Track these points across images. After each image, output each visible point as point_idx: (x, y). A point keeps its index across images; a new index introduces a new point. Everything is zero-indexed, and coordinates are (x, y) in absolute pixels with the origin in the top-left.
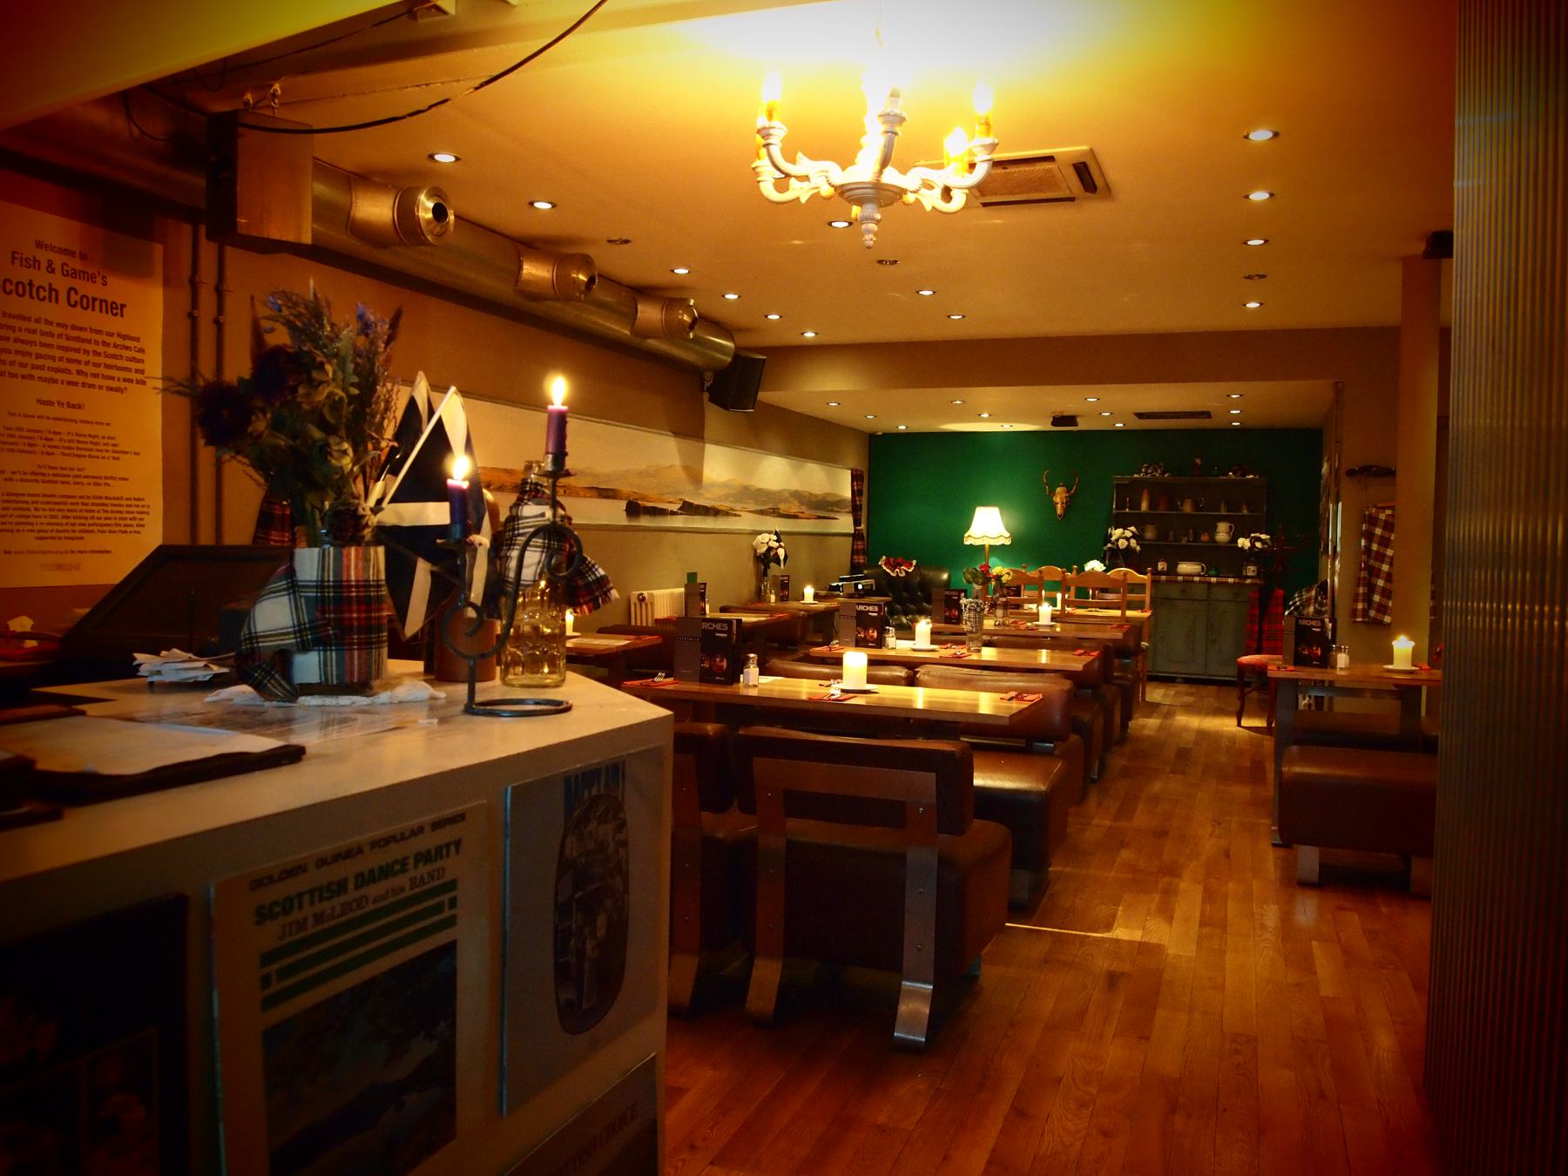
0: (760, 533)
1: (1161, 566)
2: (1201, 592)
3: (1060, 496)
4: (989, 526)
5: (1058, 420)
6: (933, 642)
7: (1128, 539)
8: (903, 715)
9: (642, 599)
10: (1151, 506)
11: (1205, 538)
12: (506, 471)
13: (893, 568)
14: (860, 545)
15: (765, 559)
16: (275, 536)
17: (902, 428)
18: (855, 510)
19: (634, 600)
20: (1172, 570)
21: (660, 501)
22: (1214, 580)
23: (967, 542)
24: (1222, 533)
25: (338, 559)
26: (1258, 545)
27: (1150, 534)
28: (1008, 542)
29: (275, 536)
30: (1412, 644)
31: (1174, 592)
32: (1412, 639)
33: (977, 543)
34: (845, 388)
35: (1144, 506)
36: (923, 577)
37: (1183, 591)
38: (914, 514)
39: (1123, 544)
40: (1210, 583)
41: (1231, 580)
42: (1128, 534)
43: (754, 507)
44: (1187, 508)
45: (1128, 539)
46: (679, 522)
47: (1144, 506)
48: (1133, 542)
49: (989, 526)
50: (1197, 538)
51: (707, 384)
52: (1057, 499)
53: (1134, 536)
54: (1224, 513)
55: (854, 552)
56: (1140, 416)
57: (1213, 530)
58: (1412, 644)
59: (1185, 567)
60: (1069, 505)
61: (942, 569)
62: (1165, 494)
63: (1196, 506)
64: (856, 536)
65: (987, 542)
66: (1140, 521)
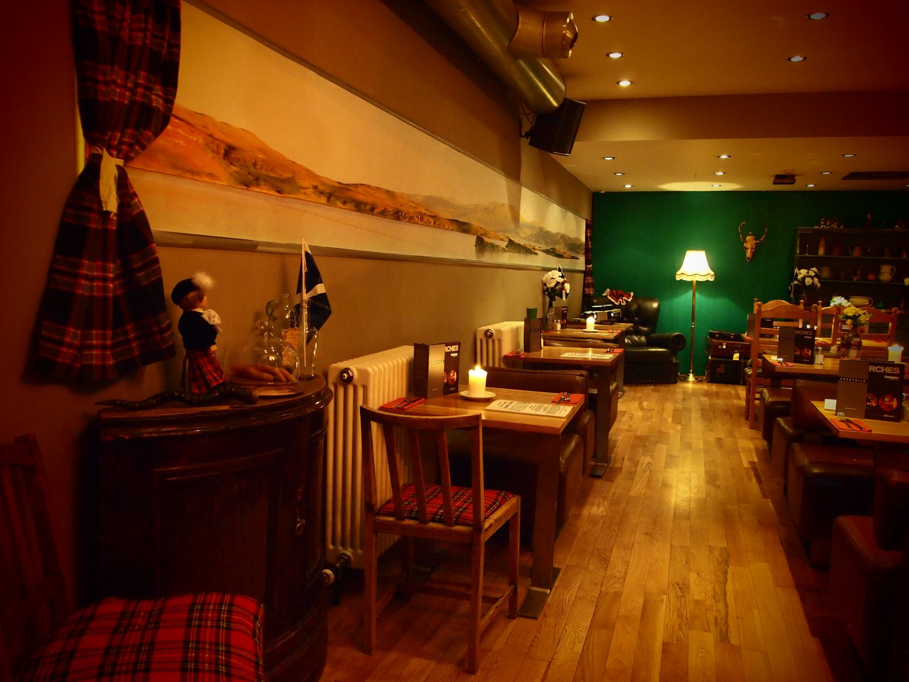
0: (550, 270)
3: (750, 243)
4: (696, 265)
5: (780, 179)
7: (812, 278)
9: (488, 335)
10: (826, 253)
11: (871, 277)
12: (388, 192)
13: (617, 298)
14: (590, 280)
15: (553, 293)
16: (88, 268)
17: (628, 186)
18: (587, 252)
19: (480, 336)
21: (496, 238)
24: (886, 274)
27: (825, 274)
28: (711, 279)
29: (88, 268)
30: (902, 348)
32: (901, 345)
33: (684, 278)
34: (641, 139)
35: (821, 252)
36: (639, 307)
38: (630, 256)
39: (808, 281)
42: (812, 273)
43: (544, 247)
44: (857, 253)
45: (812, 278)
46: (506, 258)
47: (821, 252)
48: (816, 280)
49: (696, 265)
51: (526, 127)
53: (817, 275)
54: (887, 257)
55: (585, 285)
56: (853, 176)
57: (878, 272)
58: (902, 348)
61: (652, 299)
64: (586, 273)
65: (694, 279)
66: (817, 262)
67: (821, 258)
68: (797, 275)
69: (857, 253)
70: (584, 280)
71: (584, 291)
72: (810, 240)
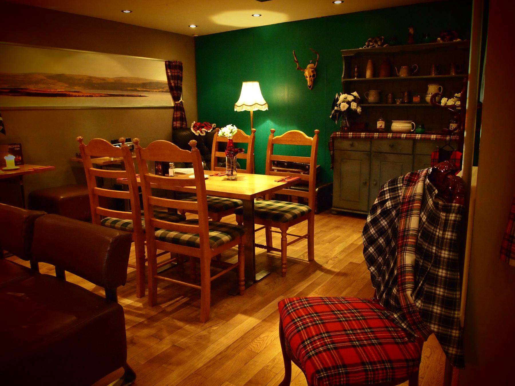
1: (380, 124)
2: (407, 147)
6: (16, 164)
7: (349, 103)
8: (148, 81)
10: (375, 74)
20: (388, 128)
22: (418, 136)
23: (237, 109)
25: (408, 250)
26: (380, 124)
27: (372, 98)
31: (385, 147)
35: (368, 74)
37: (392, 146)
40: (414, 140)
41: (433, 137)
42: (350, 98)
44: (403, 73)
45: (349, 103)
47: (368, 74)
48: (354, 105)
50: (410, 101)
52: (307, 73)
55: (175, 119)
59: (397, 126)
60: (316, 76)
62: (386, 63)
63: (411, 72)
67: (369, 81)
68: (338, 100)
69: (403, 73)
70: (174, 114)
71: (173, 124)
72: (354, 63)
